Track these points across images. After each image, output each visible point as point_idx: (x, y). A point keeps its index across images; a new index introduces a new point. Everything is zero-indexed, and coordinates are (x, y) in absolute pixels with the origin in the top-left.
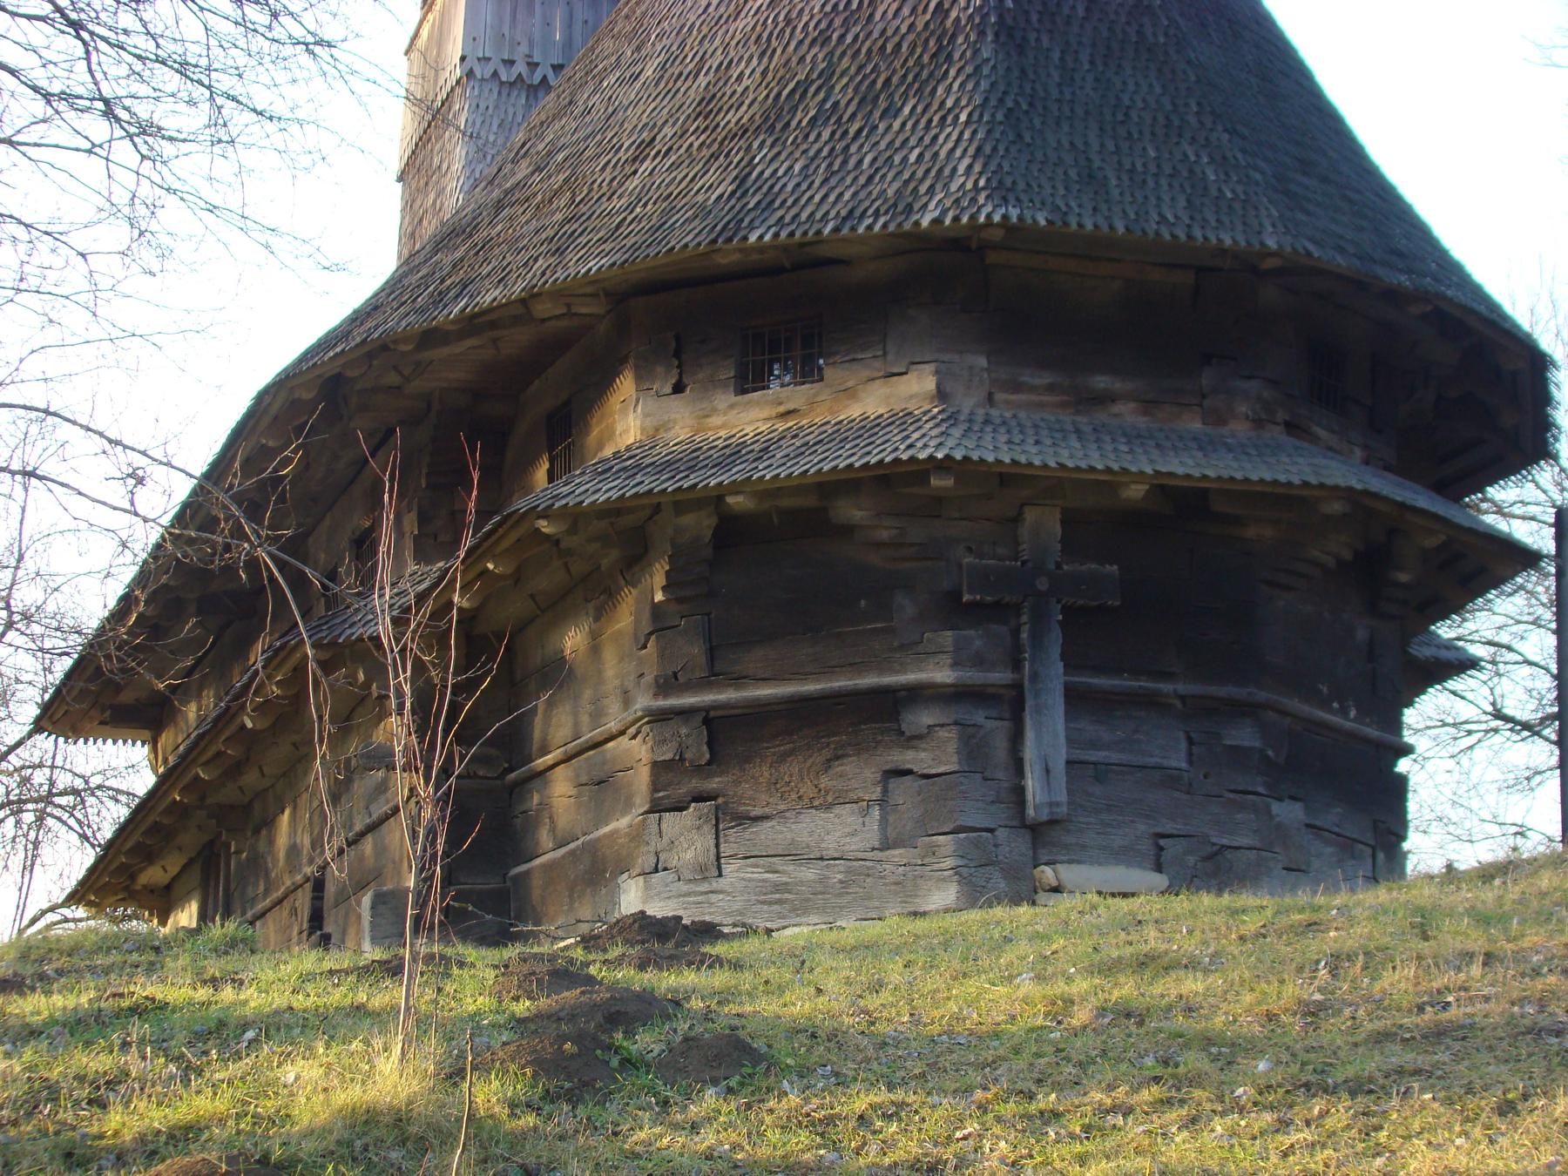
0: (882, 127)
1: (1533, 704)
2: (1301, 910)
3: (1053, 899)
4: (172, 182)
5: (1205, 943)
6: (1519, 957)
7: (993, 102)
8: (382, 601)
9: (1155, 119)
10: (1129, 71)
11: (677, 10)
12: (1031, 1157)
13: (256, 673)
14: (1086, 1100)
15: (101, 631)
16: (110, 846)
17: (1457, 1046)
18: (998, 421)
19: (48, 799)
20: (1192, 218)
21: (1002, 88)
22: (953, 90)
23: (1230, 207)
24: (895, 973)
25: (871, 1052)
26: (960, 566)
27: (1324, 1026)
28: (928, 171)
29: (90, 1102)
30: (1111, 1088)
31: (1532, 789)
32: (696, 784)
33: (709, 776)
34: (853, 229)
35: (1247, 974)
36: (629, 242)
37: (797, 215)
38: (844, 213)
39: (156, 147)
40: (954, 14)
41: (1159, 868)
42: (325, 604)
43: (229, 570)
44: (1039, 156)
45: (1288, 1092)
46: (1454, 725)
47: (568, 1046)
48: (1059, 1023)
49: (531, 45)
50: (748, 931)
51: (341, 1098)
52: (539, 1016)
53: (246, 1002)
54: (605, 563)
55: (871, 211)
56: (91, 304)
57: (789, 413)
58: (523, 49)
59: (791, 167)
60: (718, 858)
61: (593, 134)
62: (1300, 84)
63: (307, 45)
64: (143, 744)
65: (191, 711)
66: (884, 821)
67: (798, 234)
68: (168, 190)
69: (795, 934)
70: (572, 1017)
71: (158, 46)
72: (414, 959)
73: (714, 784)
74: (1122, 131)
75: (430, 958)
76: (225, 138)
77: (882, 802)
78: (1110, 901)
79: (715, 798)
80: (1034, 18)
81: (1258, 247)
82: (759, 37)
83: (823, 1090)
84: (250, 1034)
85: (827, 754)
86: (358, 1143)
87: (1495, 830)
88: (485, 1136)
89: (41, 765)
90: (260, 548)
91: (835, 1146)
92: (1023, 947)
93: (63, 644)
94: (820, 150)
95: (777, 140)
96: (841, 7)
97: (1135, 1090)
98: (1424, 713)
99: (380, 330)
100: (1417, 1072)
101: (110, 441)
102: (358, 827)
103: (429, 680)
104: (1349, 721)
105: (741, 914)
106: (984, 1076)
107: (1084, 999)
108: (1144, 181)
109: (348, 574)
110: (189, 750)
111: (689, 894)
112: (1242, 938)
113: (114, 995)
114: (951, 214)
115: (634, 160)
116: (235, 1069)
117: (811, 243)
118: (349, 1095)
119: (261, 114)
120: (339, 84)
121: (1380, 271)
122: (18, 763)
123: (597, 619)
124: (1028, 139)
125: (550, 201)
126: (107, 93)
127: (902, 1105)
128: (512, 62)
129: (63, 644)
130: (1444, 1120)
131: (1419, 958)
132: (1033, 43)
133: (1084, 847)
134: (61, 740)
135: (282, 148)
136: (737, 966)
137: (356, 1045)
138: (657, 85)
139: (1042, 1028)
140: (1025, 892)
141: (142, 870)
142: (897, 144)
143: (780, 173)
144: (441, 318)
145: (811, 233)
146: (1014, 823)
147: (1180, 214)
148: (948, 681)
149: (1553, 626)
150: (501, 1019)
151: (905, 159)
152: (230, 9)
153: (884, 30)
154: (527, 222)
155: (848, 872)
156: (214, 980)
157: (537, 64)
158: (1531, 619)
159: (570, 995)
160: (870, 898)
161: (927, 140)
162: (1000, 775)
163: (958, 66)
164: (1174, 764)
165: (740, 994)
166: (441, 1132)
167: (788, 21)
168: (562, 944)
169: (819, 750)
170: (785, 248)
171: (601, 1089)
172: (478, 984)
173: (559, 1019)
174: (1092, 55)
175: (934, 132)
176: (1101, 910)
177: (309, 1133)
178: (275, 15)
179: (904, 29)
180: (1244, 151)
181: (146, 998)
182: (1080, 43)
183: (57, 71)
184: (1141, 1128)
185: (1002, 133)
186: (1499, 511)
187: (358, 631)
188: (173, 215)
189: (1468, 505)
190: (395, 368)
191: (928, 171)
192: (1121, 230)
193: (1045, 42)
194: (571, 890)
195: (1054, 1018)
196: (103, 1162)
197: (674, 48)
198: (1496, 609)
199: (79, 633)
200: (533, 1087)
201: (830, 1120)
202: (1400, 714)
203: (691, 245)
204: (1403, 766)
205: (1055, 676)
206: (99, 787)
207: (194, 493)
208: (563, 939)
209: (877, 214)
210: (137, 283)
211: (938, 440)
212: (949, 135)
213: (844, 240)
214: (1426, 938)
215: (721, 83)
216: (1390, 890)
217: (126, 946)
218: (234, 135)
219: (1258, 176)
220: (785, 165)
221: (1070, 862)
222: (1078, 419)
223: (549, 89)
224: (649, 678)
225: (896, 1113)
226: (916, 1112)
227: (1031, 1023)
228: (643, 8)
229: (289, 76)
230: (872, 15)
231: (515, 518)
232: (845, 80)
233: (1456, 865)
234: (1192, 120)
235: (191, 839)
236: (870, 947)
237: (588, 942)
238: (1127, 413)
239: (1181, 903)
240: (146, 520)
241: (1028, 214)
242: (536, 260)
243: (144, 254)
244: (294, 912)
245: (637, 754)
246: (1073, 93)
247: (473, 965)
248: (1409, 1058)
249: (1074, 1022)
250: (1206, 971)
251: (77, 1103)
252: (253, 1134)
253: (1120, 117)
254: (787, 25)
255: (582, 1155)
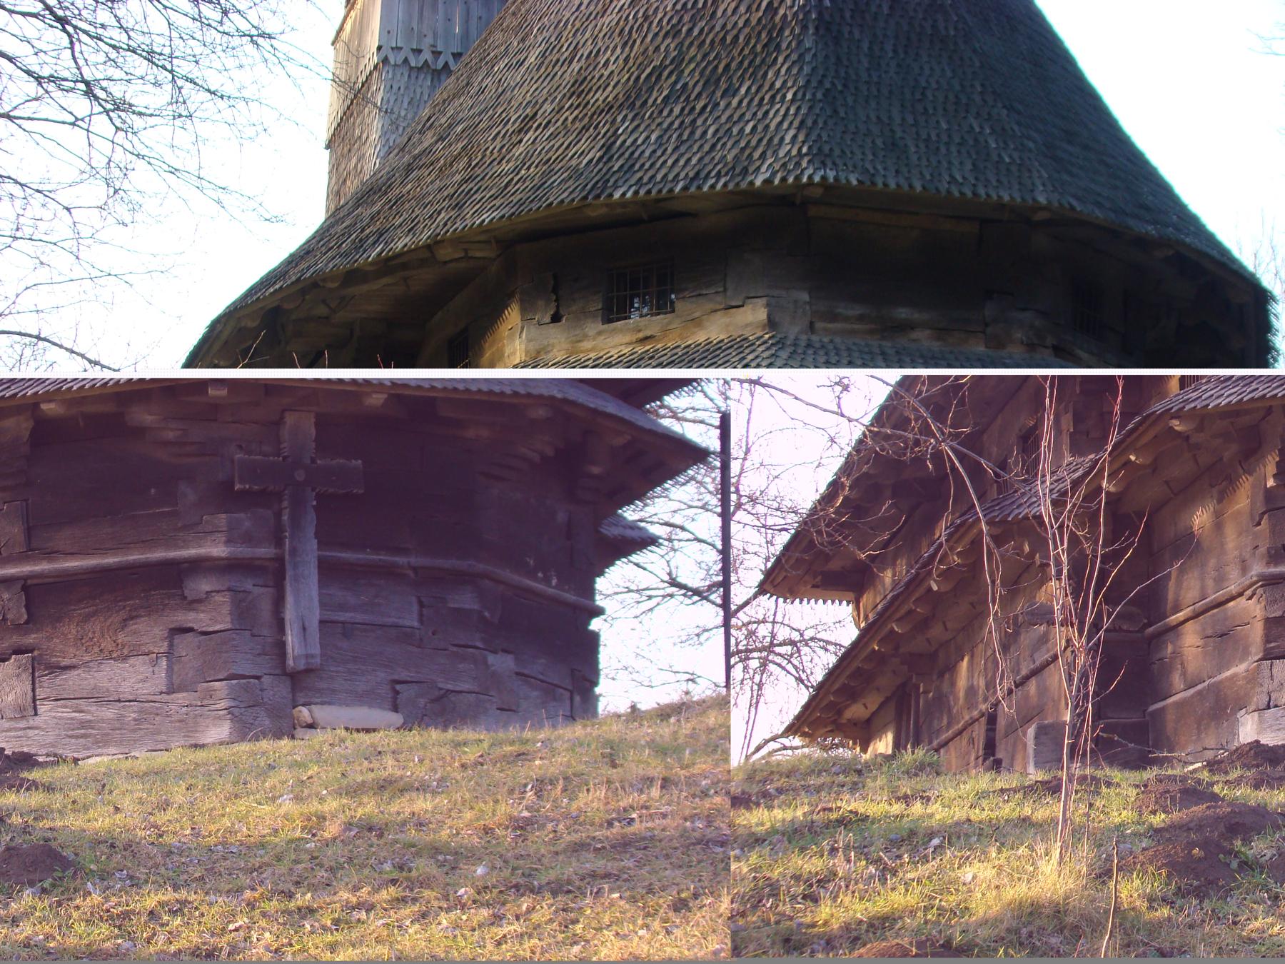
0: (723, 104)
1: (702, 574)
2: (512, 743)
3: (309, 733)
4: (141, 149)
5: (433, 770)
6: (691, 781)
7: (814, 84)
8: (1044, 487)
9: (946, 97)
10: (925, 59)
11: (554, 8)
12: (291, 945)
13: (941, 545)
14: (336, 898)
15: (814, 511)
16: (821, 687)
17: (640, 854)
18: (818, 345)
19: (770, 648)
20: (976, 179)
21: (821, 72)
22: (781, 74)
23: (1008, 170)
24: (179, 795)
25: (159, 859)
26: (232, 461)
27: (531, 838)
28: (760, 140)
29: (805, 897)
30: (356, 888)
31: (701, 644)
32: (16, 640)
33: (26, 633)
34: (699, 188)
35: (467, 796)
36: (515, 198)
37: (653, 176)
38: (691, 174)
39: (128, 120)
40: (781, 12)
41: (395, 709)
42: (998, 490)
43: (919, 461)
44: (852, 127)
45: (501, 892)
46: (637, 591)
47: (1196, 851)
48: (314, 835)
49: (435, 36)
50: (59, 760)
51: (1010, 894)
52: (1172, 827)
53: (931, 816)
54: (1227, 455)
55: (713, 173)
56: (75, 249)
57: (647, 338)
58: (429, 40)
59: (648, 137)
60: (34, 700)
61: (486, 110)
62: (1066, 69)
63: (251, 37)
64: (848, 603)
65: (888, 577)
66: (170, 670)
67: (654, 192)
68: (138, 156)
69: (96, 762)
70: (1200, 828)
71: (129, 38)
72: (1070, 780)
73: (31, 639)
74: (920, 108)
75: (1083, 779)
76: (184, 113)
77: (169, 654)
78: (355, 735)
79: (31, 651)
80: (848, 14)
81: (1030, 202)
82: (622, 30)
83: (120, 891)
84: (936, 842)
85: (123, 614)
86: (1024, 931)
87: (671, 677)
88: (1128, 925)
89: (764, 621)
90: (944, 443)
91: (130, 937)
92: (284, 773)
93: (783, 522)
94: (672, 123)
95: (636, 115)
96: (689, 6)
97: (376, 890)
98: (613, 583)
99: (312, 270)
100: (607, 876)
101: (90, 362)
102: (1024, 672)
103: (1082, 551)
104: (551, 588)
105: (53, 746)
106: (253, 879)
107: (334, 816)
108: (938, 149)
109: (1016, 464)
110: (886, 609)
111: (10, 730)
112: (463, 766)
113: (824, 809)
114: (779, 176)
115: (520, 131)
116: (923, 870)
117: (665, 199)
118: (1017, 892)
119: (214, 93)
120: (278, 69)
121: (1131, 222)
122: (746, 619)
123: (1220, 501)
124: (842, 114)
125: (451, 165)
126: (88, 76)
127: (185, 903)
128: (420, 51)
129: (783, 522)
130: (629, 915)
131: (609, 782)
132: (847, 36)
133: (333, 691)
134: (781, 600)
135: (231, 122)
136: (50, 788)
137: (1022, 851)
138: (538, 69)
139: (300, 839)
140: (286, 728)
141: (847, 707)
142: (735, 118)
143: (639, 142)
144: (361, 261)
145: (664, 191)
146: (278, 671)
147: (967, 175)
148: (223, 555)
149: (719, 510)
150: (1141, 829)
151: (742, 130)
152: (189, 7)
153: (725, 24)
154: (432, 182)
155: (141, 711)
156: (906, 797)
157: (440, 53)
158: (700, 504)
159: (1198, 810)
160: (159, 733)
161: (760, 115)
162: (265, 632)
163: (785, 54)
164: (407, 623)
165: (52, 812)
166: (1092, 921)
167: (646, 17)
168: (1191, 768)
169: (117, 612)
170: (644, 204)
171: (1223, 886)
172: (1122, 800)
173: (1189, 829)
174: (894, 45)
175: (765, 108)
176: (348, 743)
177: (984, 923)
178: (225, 13)
179: (740, 24)
180: (1019, 123)
181: (851, 812)
182: (885, 36)
183: (47, 59)
184: (381, 922)
185: (821, 109)
186: (675, 416)
187: (1024, 511)
188: (141, 176)
189: (648, 411)
190: (324, 302)
191: (760, 140)
192: (919, 188)
193: (857, 34)
194: (1199, 724)
195: (310, 831)
196: (815, 946)
197: (553, 39)
198: (671, 496)
199: (796, 512)
200: (1167, 885)
201: (126, 915)
202: (594, 582)
203: (567, 201)
204: (595, 624)
205: (311, 551)
206: (812, 639)
207: (890, 398)
208: (1192, 763)
209: (718, 176)
210: (112, 232)
211: (769, 361)
212: (778, 110)
213: (692, 197)
214: (614, 766)
215: (591, 68)
216: (585, 726)
217: (834, 769)
218: (192, 111)
219: (1031, 145)
220: (644, 136)
221: (323, 703)
222: (884, 343)
223: (450, 73)
224: (1263, 550)
225: (180, 909)
226: (197, 908)
227: (290, 835)
228: (527, 6)
229: (237, 63)
230: (714, 12)
231: (1153, 417)
232: (692, 66)
233: (639, 706)
234: (977, 98)
235: (887, 681)
236: (159, 773)
237: (1213, 766)
238: (923, 338)
239: (413, 737)
240: (850, 420)
241: (842, 176)
242: (439, 213)
243: (118, 208)
244: (972, 741)
245: (1252, 611)
246: (880, 76)
247: (1118, 785)
248: (600, 864)
249: (326, 835)
250: (434, 793)
251: (794, 898)
252: (938, 923)
253: (918, 96)
254: (645, 20)
255: (1208, 940)
